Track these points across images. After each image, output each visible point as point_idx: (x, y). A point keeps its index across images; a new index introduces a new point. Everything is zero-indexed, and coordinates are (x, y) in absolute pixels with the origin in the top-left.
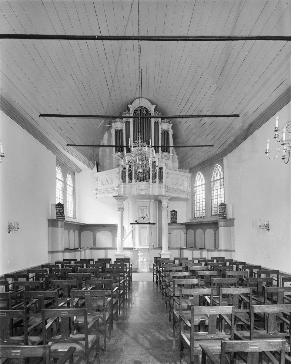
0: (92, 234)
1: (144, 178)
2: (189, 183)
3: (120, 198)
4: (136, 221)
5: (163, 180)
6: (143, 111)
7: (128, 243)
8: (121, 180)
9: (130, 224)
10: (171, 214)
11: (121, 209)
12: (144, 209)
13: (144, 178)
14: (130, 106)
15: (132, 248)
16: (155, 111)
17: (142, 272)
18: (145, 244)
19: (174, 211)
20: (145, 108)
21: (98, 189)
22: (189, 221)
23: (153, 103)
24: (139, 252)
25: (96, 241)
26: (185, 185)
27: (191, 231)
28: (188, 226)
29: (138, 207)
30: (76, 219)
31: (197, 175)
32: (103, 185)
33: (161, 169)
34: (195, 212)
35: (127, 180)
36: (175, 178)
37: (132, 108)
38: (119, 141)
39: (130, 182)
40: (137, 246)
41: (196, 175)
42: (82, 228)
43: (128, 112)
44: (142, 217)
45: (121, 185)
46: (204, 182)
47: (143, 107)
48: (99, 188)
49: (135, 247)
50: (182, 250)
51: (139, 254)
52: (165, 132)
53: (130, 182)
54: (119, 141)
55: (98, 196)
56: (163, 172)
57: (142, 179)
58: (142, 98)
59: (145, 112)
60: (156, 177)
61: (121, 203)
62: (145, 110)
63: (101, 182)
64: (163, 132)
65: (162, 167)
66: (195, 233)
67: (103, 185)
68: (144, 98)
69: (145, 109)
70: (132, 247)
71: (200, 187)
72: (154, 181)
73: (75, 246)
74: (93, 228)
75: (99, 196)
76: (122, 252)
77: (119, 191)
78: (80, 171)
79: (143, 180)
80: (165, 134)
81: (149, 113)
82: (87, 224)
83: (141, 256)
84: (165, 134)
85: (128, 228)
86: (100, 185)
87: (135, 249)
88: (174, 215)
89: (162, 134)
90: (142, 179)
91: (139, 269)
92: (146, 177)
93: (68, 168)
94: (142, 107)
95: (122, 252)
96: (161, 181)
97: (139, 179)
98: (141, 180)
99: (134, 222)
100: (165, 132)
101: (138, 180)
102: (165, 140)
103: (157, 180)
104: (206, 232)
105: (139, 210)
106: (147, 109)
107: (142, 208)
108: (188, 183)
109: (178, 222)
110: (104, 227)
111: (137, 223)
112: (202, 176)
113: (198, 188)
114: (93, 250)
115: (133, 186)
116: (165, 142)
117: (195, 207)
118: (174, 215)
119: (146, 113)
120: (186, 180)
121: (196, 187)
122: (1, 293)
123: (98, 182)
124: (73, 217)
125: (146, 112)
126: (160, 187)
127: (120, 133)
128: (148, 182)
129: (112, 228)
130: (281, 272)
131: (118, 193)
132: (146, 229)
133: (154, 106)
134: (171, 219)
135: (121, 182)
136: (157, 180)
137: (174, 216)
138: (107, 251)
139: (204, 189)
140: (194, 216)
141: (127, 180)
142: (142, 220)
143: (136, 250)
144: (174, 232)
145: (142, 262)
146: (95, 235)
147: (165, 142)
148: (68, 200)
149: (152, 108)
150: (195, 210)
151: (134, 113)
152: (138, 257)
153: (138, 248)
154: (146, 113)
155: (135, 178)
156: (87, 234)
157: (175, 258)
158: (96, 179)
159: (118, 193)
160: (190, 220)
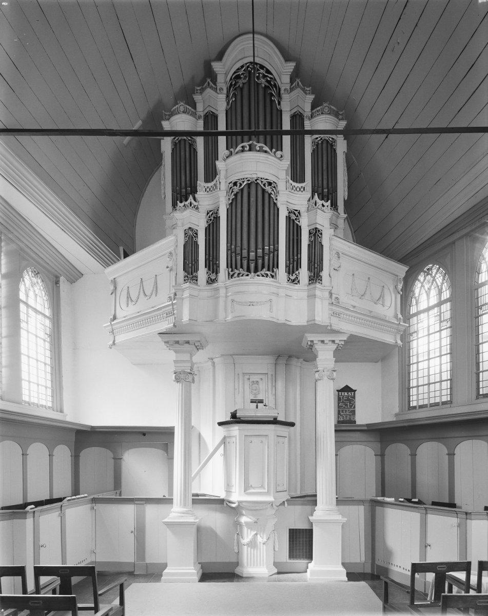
0: (110, 454)
1: (260, 261)
2: (399, 296)
3: (178, 338)
4: (234, 415)
5: (324, 274)
6: (258, 78)
7: (212, 483)
8: (181, 273)
9: (220, 424)
10: (339, 399)
11: (185, 377)
12: (260, 382)
13: (260, 261)
14: (217, 66)
15: (221, 501)
16: (292, 81)
17: (249, 578)
18: (262, 487)
19: (347, 389)
20: (262, 67)
21: (118, 315)
22: (390, 418)
23: (287, 59)
24: (244, 512)
25: (120, 471)
26: (387, 303)
27: (399, 450)
28: (385, 435)
29: (241, 376)
30: (61, 411)
31: (421, 278)
32: (132, 301)
33: (315, 233)
34: (413, 392)
35: (202, 273)
36: (349, 284)
37: (224, 70)
38: (183, 172)
39: (211, 281)
40: (236, 497)
41: (416, 279)
42: (84, 438)
43: (211, 83)
44: (252, 402)
45: (183, 290)
46: (446, 295)
47: (257, 64)
48: (120, 314)
49: (232, 499)
50: (378, 509)
51: (244, 519)
52: (325, 145)
53: (211, 281)
54: (183, 172)
55: (116, 338)
56: (322, 246)
57: (252, 266)
58: (253, 33)
59: (263, 81)
60: (299, 265)
61: (186, 357)
62: (264, 76)
63: (125, 293)
64: (317, 145)
65: (319, 227)
66: (413, 455)
67: (130, 302)
68: (261, 34)
69: (261, 71)
70: (222, 495)
71: (431, 312)
72: (293, 278)
73: (55, 491)
74: (112, 439)
75: (120, 339)
76: (186, 513)
77: (175, 312)
78: (75, 275)
79: (256, 271)
80: (325, 152)
81: (275, 85)
82: (92, 427)
83: (247, 523)
84: (325, 152)
85: (212, 435)
86: (124, 306)
87: (230, 502)
88: (348, 400)
89: (315, 153)
90: (252, 266)
91: (242, 566)
92: (266, 258)
93: (27, 254)
94: (254, 63)
95: (186, 513)
96: (315, 276)
97: (242, 267)
98: (249, 270)
99: (228, 419)
100: (325, 145)
101: (237, 272)
102: (325, 167)
103: (304, 273)
104: (457, 451)
105: (243, 384)
106: (268, 71)
107: (255, 378)
108: (396, 298)
109: (358, 423)
110: (144, 434)
111: (235, 419)
112: (439, 279)
113: (423, 316)
114: (100, 507)
115: (222, 292)
116: (325, 177)
117: (413, 375)
118: (348, 400)
119: (267, 84)
120: (392, 288)
121: (418, 313)
122: (1, 567)
123: (118, 295)
124: (50, 404)
125: (267, 81)
126: (312, 296)
127: (187, 149)
128: (273, 277)
129: (158, 438)
130: (468, 524)
131: (172, 319)
132: (264, 439)
133: (291, 66)
134: (339, 413)
135: (182, 279)
136: (304, 273)
137: (346, 405)
138: (144, 511)
139: (447, 315)
140: (409, 402)
141: (202, 273)
142: (250, 411)
143: (234, 505)
144: (348, 450)
145: (253, 544)
146: (117, 460)
147: (325, 177)
148: (22, 351)
149: (283, 72)
150: (413, 383)
151: (231, 85)
152: (241, 531)
153: (240, 502)
154: (267, 84)
155: (230, 265)
156: (92, 456)
157: (414, 565)
158: (112, 288)
159: (172, 319)
160: (396, 415)
